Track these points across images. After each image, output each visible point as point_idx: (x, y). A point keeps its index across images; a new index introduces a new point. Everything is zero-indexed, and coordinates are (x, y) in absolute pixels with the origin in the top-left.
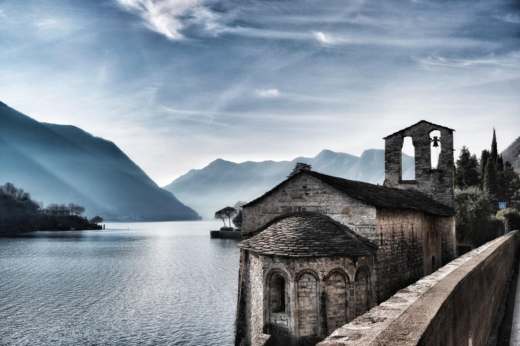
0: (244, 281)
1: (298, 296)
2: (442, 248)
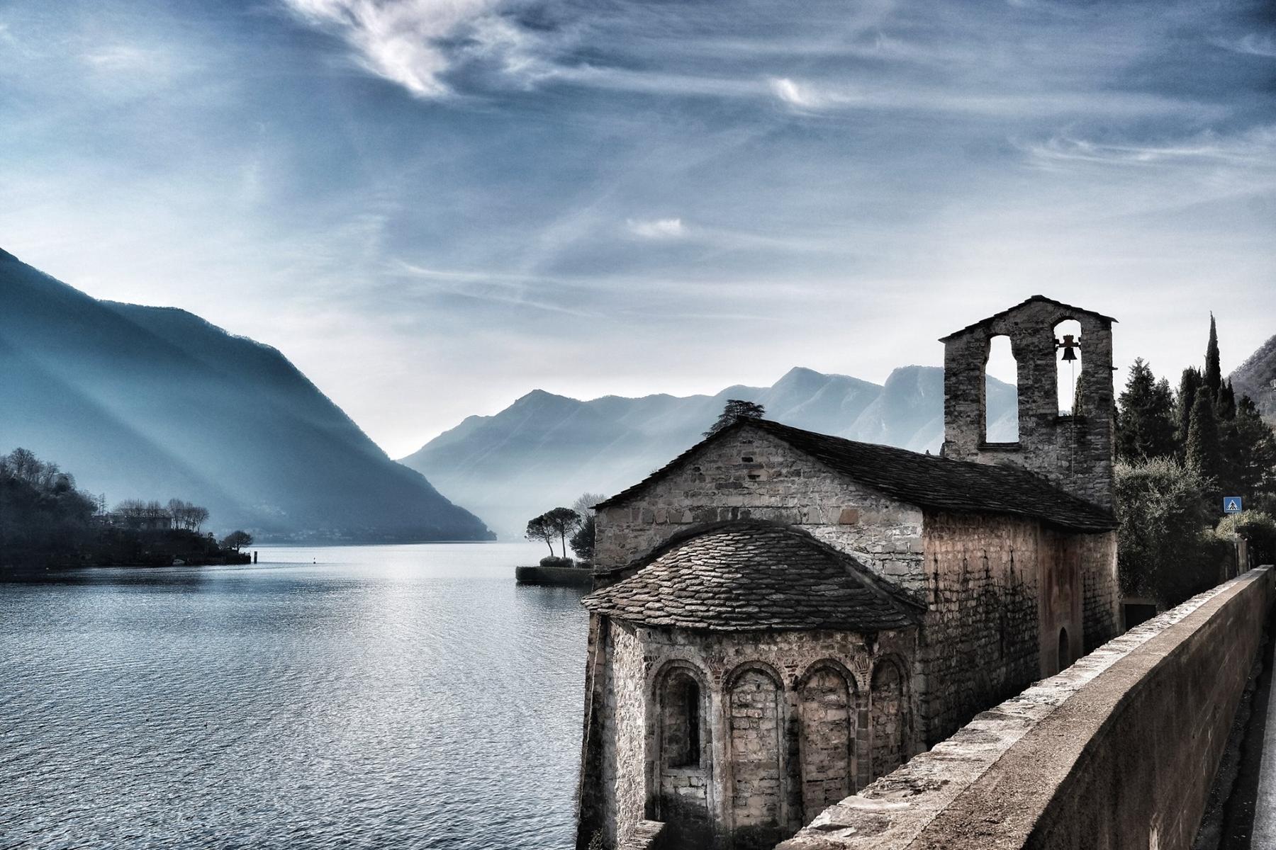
0: (599, 689)
1: (732, 728)
2: (1085, 610)
